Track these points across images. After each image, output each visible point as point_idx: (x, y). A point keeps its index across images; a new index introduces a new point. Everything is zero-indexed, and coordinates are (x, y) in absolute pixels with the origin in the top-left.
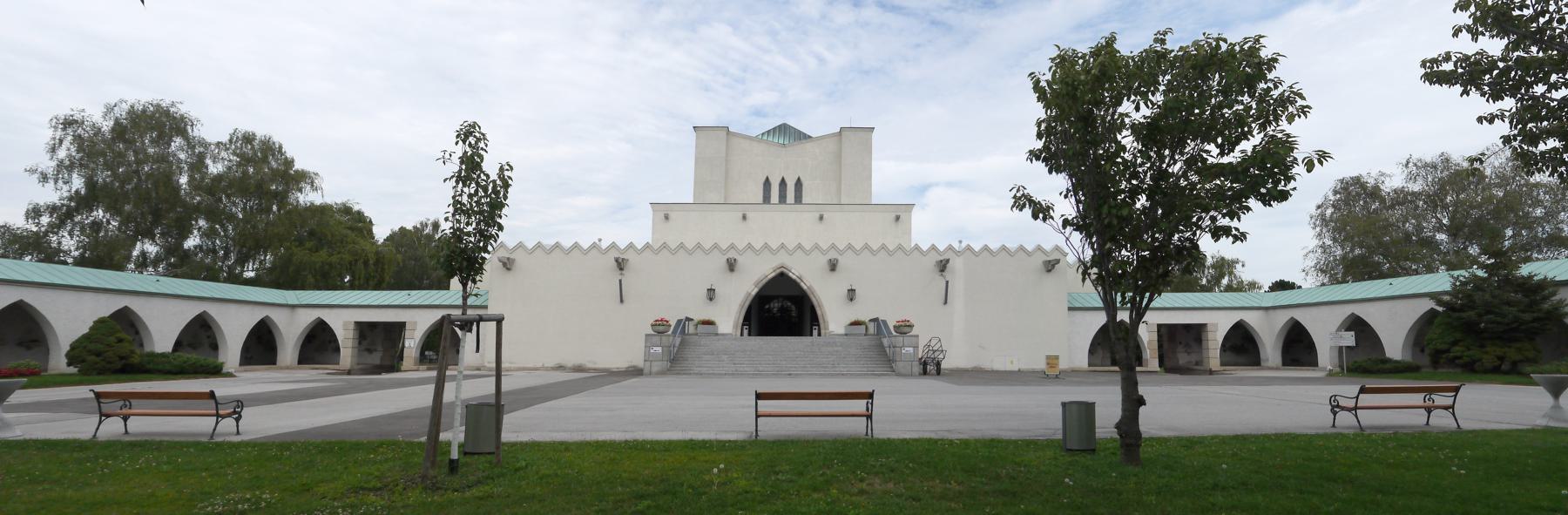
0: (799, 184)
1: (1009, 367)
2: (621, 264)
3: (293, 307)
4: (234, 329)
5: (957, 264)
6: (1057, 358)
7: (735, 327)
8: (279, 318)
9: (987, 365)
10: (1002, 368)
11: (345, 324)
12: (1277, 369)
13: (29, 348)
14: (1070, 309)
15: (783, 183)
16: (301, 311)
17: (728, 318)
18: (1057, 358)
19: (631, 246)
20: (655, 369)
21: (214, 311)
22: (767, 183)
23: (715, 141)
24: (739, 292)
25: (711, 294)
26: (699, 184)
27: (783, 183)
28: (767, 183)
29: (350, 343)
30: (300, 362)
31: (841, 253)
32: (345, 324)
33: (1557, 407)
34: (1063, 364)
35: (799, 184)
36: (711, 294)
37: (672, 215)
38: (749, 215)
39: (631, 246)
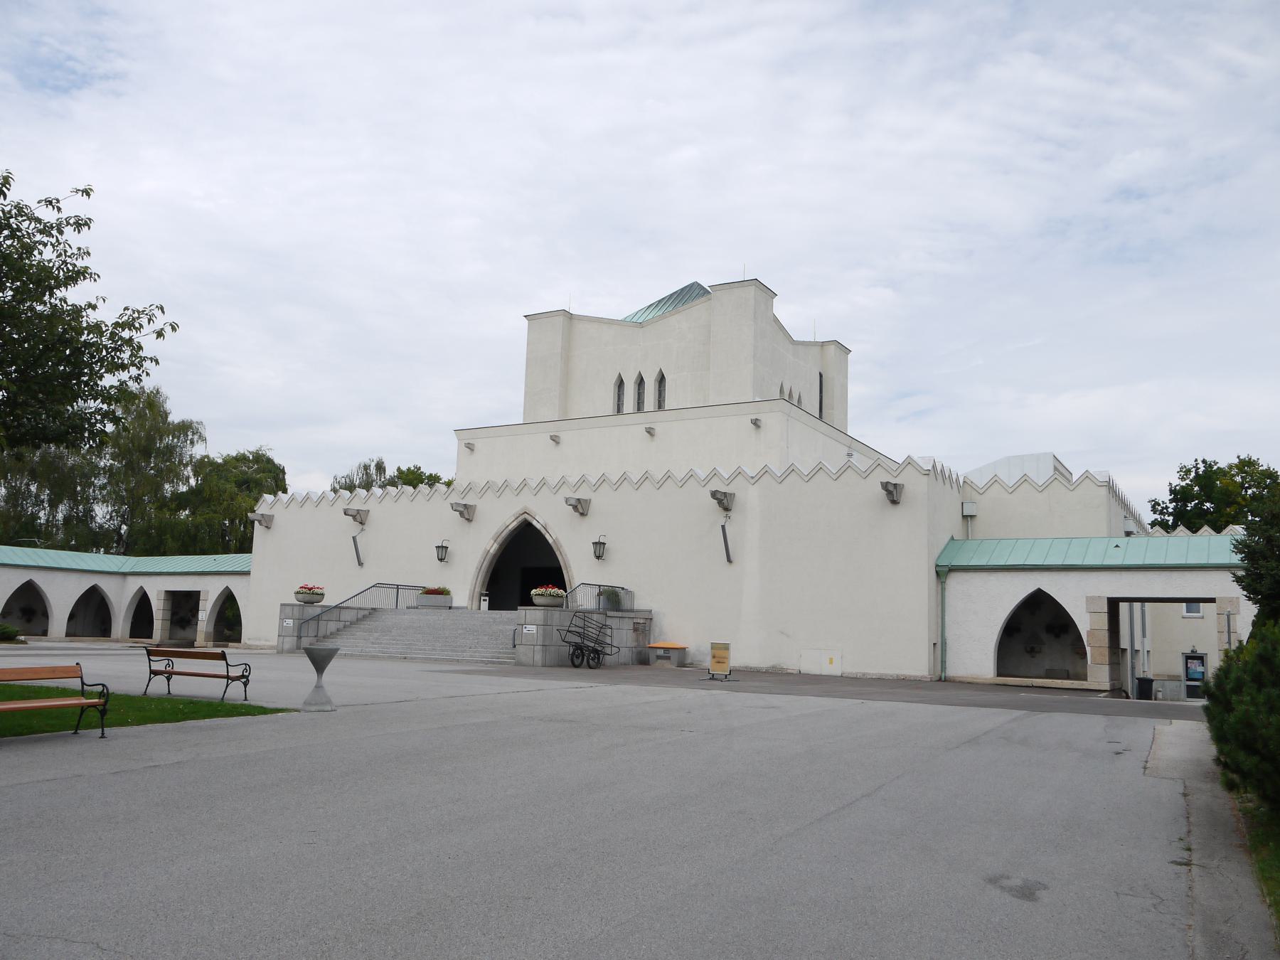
0: (661, 380)
1: (827, 670)
2: (724, 501)
3: (125, 574)
4: (61, 598)
5: (749, 498)
6: (726, 647)
7: (472, 599)
8: (109, 587)
9: (792, 663)
10: (814, 670)
11: (159, 592)
12: (1133, 674)
13: (1057, 636)
14: (247, 573)
15: (641, 382)
16: (131, 579)
17: (463, 584)
18: (726, 647)
19: (739, 473)
20: (287, 646)
21: (40, 579)
22: (620, 384)
23: (558, 332)
24: (477, 547)
25: (443, 553)
26: (532, 396)
27: (641, 382)
28: (620, 384)
29: (160, 617)
30: (67, 635)
31: (596, 487)
32: (1090, 600)
34: (737, 659)
35: (661, 380)
36: (443, 553)
37: (479, 445)
38: (564, 436)
39: (739, 473)
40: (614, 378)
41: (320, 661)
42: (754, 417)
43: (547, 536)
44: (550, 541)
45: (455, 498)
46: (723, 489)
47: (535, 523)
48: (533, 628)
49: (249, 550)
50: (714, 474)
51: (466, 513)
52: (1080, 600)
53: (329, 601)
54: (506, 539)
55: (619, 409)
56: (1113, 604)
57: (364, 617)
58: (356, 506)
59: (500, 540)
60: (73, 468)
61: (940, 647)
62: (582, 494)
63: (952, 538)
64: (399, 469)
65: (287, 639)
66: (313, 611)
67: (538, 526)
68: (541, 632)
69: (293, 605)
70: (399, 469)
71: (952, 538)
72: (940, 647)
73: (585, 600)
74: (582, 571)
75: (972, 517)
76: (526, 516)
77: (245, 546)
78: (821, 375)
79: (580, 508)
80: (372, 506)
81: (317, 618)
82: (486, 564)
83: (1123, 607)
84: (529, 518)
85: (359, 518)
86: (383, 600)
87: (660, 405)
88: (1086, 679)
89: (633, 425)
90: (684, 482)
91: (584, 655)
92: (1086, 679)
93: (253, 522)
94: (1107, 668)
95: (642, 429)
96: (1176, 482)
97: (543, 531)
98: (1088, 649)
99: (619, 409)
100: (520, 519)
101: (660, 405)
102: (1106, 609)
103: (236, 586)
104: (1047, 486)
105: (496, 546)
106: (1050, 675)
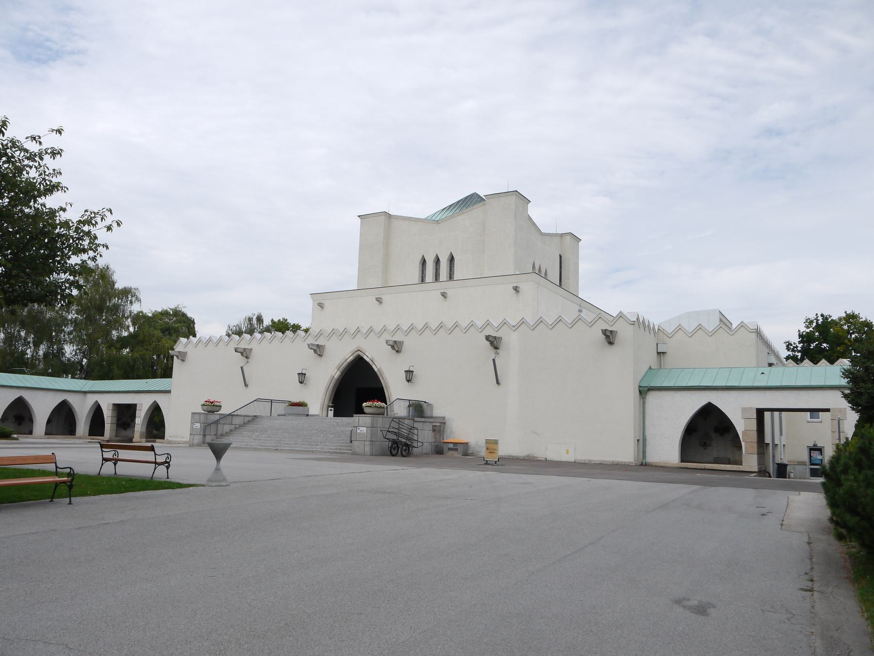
0: (452, 259)
1: (565, 458)
2: (494, 343)
3: (85, 393)
4: (42, 408)
5: (511, 340)
6: (496, 442)
7: (322, 409)
8: (74, 401)
9: (541, 453)
10: (556, 458)
11: (108, 404)
14: (169, 392)
15: (437, 261)
16: (89, 396)
17: (316, 399)
18: (496, 442)
19: (504, 323)
20: (196, 442)
21: (28, 396)
22: (424, 262)
23: (381, 227)
24: (326, 374)
25: (302, 378)
26: (363, 270)
27: (437, 261)
28: (424, 262)
29: (109, 421)
30: (46, 434)
31: (407, 333)
32: (744, 410)
33: (217, 469)
34: (504, 450)
35: (452, 259)
36: (302, 378)
37: (327, 304)
38: (385, 298)
39: (504, 323)
40: (419, 259)
41: (218, 452)
42: (515, 285)
43: (374, 367)
44: (376, 370)
45: (311, 340)
46: (494, 334)
47: (365, 357)
48: (364, 429)
49: (170, 376)
50: (488, 324)
51: (318, 350)
52: (737, 410)
53: (224, 411)
54: (345, 369)
55: (423, 280)
56: (760, 413)
57: (249, 421)
58: (243, 345)
59: (341, 369)
60: (50, 320)
61: (642, 442)
62: (397, 338)
63: (650, 368)
64: (272, 320)
65: (196, 437)
66: (214, 417)
67: (368, 360)
68: (369, 432)
69: (200, 414)
70: (272, 320)
71: (650, 368)
72: (642, 442)
73: (400, 410)
74: (397, 390)
75: (663, 353)
76: (359, 353)
77: (167, 373)
78: (561, 257)
79: (396, 347)
80: (254, 345)
81: (217, 422)
82: (332, 385)
83: (767, 415)
84: (361, 354)
85: (245, 354)
86: (262, 410)
87: (451, 277)
88: (741, 464)
89: (432, 291)
90: (467, 329)
91: (399, 447)
92: (741, 464)
93: (172, 357)
94: (756, 457)
95: (438, 293)
96: (803, 329)
97: (371, 363)
98: (743, 444)
99: (423, 280)
100: (355, 355)
101: (451, 277)
102: (755, 416)
103: (161, 400)
104: (715, 332)
105: (338, 373)
106: (717, 461)
